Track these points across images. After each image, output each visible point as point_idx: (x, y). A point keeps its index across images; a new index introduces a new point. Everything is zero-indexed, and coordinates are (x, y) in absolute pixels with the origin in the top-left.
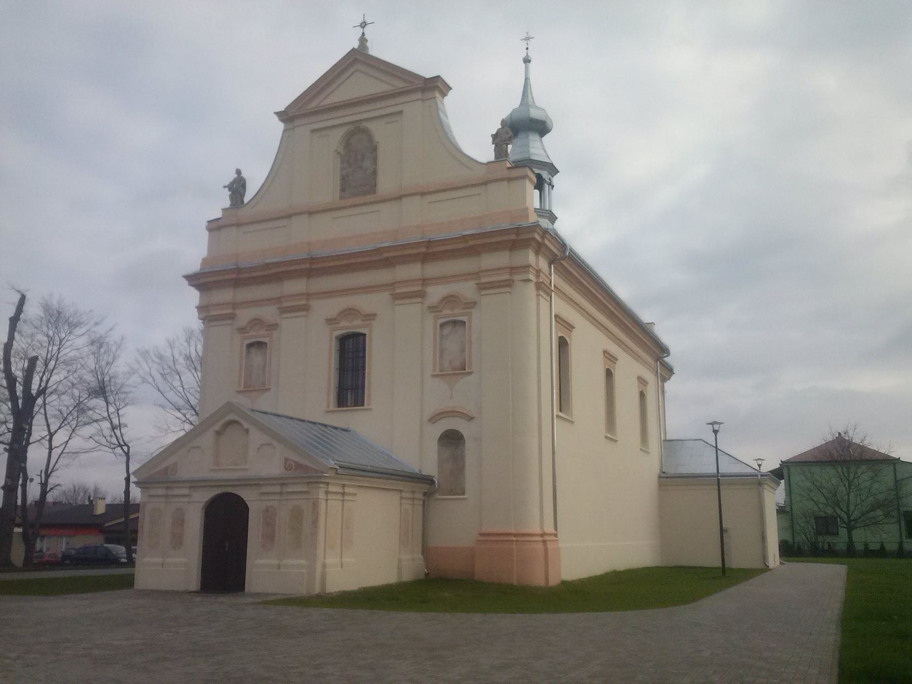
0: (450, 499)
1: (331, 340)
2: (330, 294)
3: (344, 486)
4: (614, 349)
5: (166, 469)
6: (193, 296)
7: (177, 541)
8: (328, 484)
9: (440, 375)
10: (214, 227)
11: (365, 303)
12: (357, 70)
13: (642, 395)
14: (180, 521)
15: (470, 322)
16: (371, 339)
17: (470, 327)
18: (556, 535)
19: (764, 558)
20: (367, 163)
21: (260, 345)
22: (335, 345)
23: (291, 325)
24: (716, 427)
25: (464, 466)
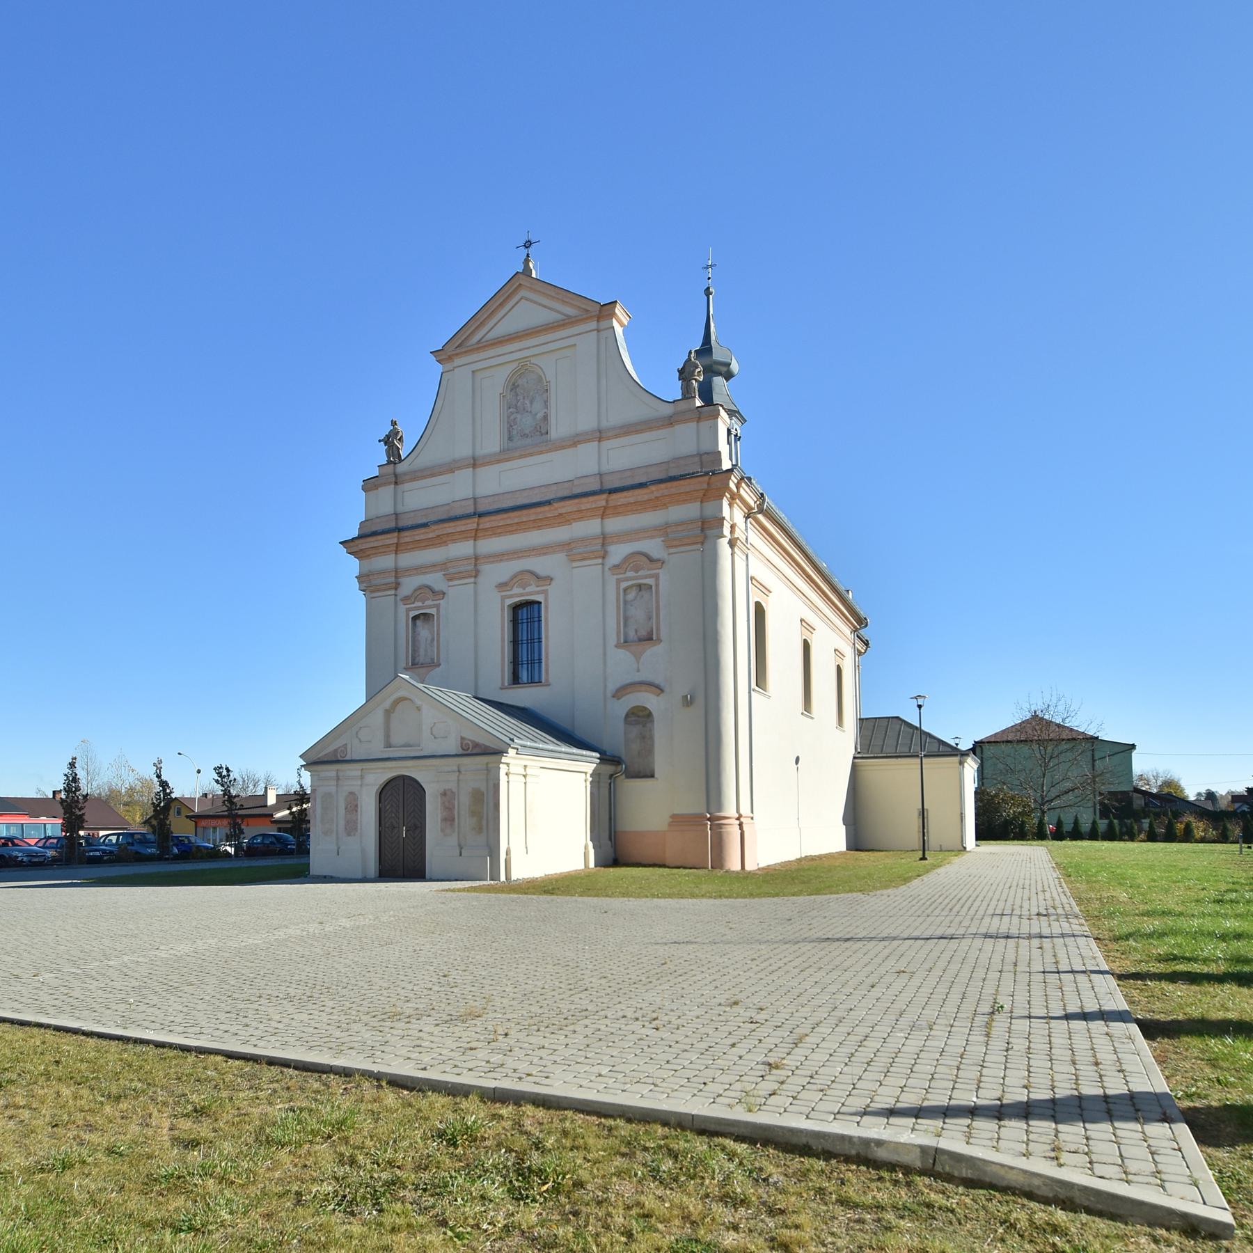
0: (508, 853)
1: (503, 609)
2: (499, 557)
4: (812, 618)
5: (336, 751)
6: (353, 565)
7: (352, 827)
9: (625, 643)
10: (370, 485)
11: (540, 565)
14: (353, 806)
15: (657, 585)
16: (546, 607)
19: (962, 840)
20: (537, 406)
21: (426, 617)
23: (459, 593)
24: (920, 702)
25: (652, 746)
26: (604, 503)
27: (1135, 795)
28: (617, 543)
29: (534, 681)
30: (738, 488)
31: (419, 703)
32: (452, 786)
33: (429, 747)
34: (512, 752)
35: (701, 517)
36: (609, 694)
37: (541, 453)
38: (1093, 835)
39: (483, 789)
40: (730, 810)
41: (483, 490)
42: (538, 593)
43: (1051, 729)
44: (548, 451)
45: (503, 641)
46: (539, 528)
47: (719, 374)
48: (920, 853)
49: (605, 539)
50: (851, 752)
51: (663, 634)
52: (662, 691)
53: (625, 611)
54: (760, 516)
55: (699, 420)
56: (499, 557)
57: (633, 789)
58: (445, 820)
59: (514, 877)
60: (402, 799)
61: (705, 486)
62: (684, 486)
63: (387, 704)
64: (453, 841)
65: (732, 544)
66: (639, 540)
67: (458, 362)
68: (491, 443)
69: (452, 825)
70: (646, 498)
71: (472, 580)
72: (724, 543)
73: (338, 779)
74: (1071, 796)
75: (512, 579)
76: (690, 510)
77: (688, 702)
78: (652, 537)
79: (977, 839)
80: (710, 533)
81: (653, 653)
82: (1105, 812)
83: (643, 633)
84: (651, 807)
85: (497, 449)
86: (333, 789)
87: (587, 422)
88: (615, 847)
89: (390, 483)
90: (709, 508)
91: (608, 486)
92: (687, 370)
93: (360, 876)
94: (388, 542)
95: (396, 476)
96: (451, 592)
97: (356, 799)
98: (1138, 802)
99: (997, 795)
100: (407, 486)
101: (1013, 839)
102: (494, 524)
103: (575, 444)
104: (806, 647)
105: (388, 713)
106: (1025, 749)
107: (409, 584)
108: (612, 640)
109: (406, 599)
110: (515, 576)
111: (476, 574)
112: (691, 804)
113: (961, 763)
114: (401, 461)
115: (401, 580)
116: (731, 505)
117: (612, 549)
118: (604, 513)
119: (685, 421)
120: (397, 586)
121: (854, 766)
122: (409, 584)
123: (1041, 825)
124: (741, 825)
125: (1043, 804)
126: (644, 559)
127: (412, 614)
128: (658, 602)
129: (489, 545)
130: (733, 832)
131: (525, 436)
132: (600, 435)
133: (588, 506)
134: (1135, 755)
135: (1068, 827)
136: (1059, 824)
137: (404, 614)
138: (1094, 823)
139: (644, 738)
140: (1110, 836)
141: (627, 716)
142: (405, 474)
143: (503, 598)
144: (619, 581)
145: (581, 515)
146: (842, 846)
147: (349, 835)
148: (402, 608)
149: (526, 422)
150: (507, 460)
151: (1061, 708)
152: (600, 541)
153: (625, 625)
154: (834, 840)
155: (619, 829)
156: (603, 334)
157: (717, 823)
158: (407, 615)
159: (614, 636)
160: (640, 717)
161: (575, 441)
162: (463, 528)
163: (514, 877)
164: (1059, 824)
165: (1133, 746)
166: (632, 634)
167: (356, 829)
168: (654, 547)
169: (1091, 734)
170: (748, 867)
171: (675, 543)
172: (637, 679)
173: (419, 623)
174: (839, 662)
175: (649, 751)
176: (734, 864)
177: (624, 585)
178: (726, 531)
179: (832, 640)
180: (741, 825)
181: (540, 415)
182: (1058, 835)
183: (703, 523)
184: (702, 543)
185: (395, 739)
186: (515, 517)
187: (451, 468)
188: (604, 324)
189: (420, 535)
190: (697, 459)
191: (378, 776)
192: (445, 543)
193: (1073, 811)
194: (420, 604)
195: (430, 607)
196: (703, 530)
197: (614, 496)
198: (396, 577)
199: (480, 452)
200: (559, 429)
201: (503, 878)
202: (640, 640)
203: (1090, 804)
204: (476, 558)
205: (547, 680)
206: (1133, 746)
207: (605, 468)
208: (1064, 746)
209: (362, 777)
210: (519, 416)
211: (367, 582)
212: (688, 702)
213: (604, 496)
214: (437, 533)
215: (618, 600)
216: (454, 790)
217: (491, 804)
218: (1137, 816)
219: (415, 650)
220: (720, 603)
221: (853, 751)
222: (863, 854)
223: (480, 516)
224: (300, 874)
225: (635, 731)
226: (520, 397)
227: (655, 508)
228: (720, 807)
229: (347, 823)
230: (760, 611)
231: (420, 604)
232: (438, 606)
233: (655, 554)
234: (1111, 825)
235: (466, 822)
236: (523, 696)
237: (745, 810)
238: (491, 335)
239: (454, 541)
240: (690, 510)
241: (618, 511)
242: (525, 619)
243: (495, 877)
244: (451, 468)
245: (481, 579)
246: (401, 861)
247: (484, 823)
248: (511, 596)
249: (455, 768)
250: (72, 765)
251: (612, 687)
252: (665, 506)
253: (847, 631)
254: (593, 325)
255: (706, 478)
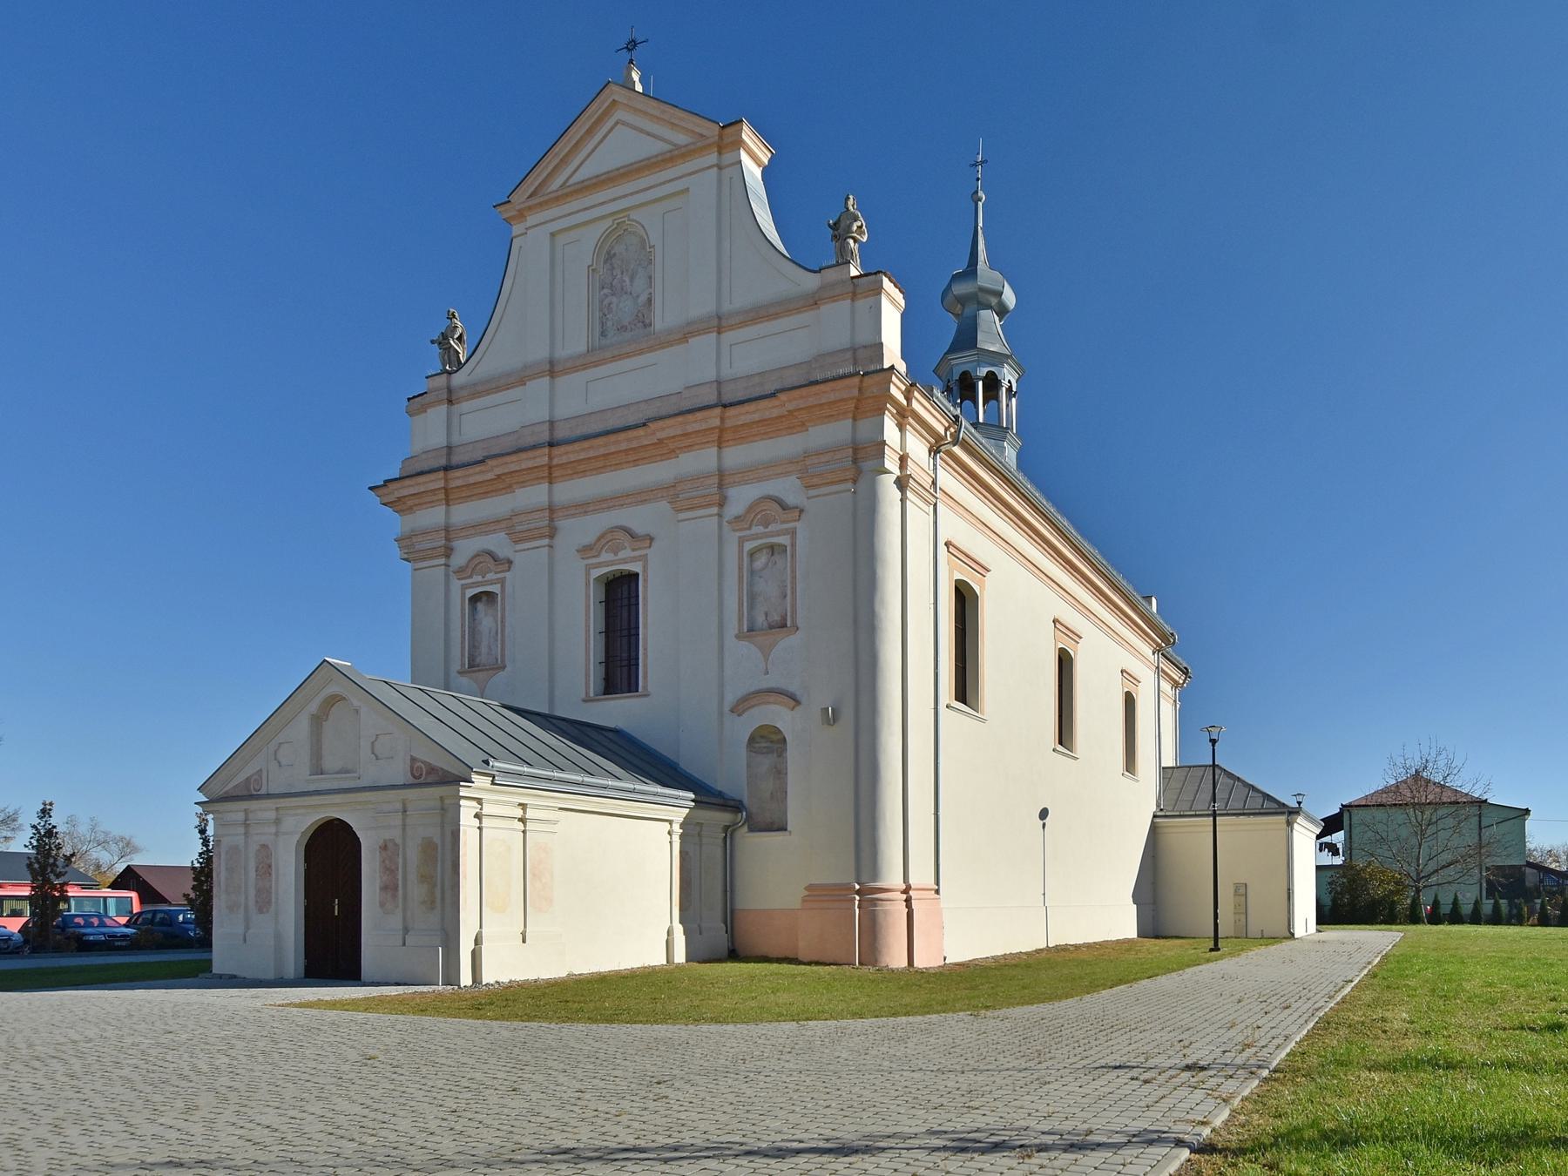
0: (478, 940)
1: (587, 585)
2: (583, 508)
3: (523, 806)
7: (265, 901)
8: (479, 801)
9: (750, 631)
11: (637, 518)
12: (617, 123)
13: (1130, 701)
14: (266, 869)
15: (793, 545)
16: (645, 581)
17: (793, 556)
18: (937, 892)
21: (490, 596)
22: (596, 595)
23: (529, 559)
26: (717, 422)
27: (1528, 870)
28: (739, 483)
29: (631, 686)
30: (908, 399)
31: (356, 703)
32: (395, 834)
33: (371, 773)
34: (480, 781)
35: (854, 441)
36: (727, 709)
37: (641, 352)
38: (1476, 918)
39: (437, 840)
40: (892, 877)
41: (562, 411)
42: (634, 559)
43: (1431, 787)
44: (651, 349)
45: (587, 631)
46: (636, 463)
47: (989, 307)
48: (1211, 945)
49: (723, 478)
50: (1153, 808)
51: (799, 622)
52: (798, 702)
53: (751, 585)
54: (957, 450)
55: (854, 296)
56: (583, 508)
57: (753, 844)
58: (384, 888)
59: (488, 977)
60: (332, 856)
61: (855, 392)
62: (828, 393)
63: (313, 707)
64: (396, 921)
65: (902, 484)
66: (768, 478)
67: (532, 219)
68: (576, 342)
69: (395, 896)
70: (775, 413)
71: (546, 541)
72: (887, 484)
73: (246, 825)
74: (1451, 870)
75: (599, 539)
76: (838, 432)
77: (831, 718)
78: (787, 474)
79: (1319, 922)
80: (867, 465)
81: (787, 644)
82: (1492, 890)
83: (776, 618)
84: (778, 875)
85: (583, 348)
86: (240, 840)
87: (701, 305)
88: (723, 928)
89: (439, 402)
90: (865, 426)
91: (727, 398)
92: (842, 225)
93: (271, 976)
94: (432, 486)
95: (450, 390)
96: (518, 559)
97: (269, 856)
98: (1531, 877)
99: (1363, 870)
100: (465, 406)
101: (1381, 923)
102: (573, 457)
103: (684, 338)
104: (1065, 663)
105: (318, 721)
106: (1399, 815)
107: (465, 548)
108: (732, 627)
109: (460, 571)
110: (602, 536)
111: (552, 533)
112: (834, 870)
113: (1290, 824)
114: (460, 366)
115: (455, 544)
116: (901, 427)
117: (732, 492)
118: (721, 439)
119: (834, 299)
120: (448, 552)
121: (1154, 829)
122: (465, 548)
123: (1415, 904)
124: (908, 901)
125: (1418, 881)
126: (776, 506)
127: (470, 593)
128: (793, 571)
129: (570, 490)
130: (895, 911)
131: (623, 329)
132: (719, 324)
133: (697, 427)
134: (1530, 824)
135: (1445, 909)
136: (1436, 904)
137: (460, 592)
138: (1477, 903)
139: (779, 772)
140: (1496, 919)
141: (752, 740)
142: (462, 388)
143: (588, 568)
144: (742, 541)
145: (688, 442)
146: (1131, 932)
147: (261, 911)
148: (456, 585)
149: (625, 308)
150: (596, 364)
151: (1441, 763)
152: (715, 480)
153: (751, 607)
154: (1122, 923)
155: (739, 905)
156: (727, 172)
157: (870, 896)
158: (463, 595)
159: (735, 622)
160: (768, 742)
161: (685, 334)
162: (530, 464)
163: (488, 977)
164: (1436, 904)
165: (1527, 811)
166: (760, 620)
167: (269, 902)
168: (788, 488)
169: (1476, 795)
170: (919, 963)
171: (815, 481)
172: (765, 685)
173: (480, 606)
174: (1130, 687)
175: (781, 794)
176: (896, 958)
177: (748, 546)
178: (891, 463)
179: (1116, 657)
180: (908, 901)
181: (643, 298)
182: (1435, 919)
183: (855, 450)
184: (855, 482)
185: (329, 763)
186: (600, 447)
187: (520, 378)
188: (728, 158)
189: (476, 475)
190: (849, 355)
191: (302, 820)
192: (509, 488)
193: (1453, 887)
194: (479, 578)
195: (492, 583)
196: (855, 461)
197: (731, 412)
198: (448, 539)
199: (561, 353)
200: (665, 318)
201: (466, 979)
202: (771, 627)
203: (1476, 878)
204: (551, 509)
205: (645, 687)
206: (1527, 811)
207: (727, 372)
208: (1442, 812)
209: (277, 822)
210: (614, 300)
211: (412, 548)
212: (831, 718)
213: (718, 411)
214: (498, 471)
215: (740, 568)
216: (399, 841)
217: (448, 864)
218: (1529, 895)
219: (474, 647)
220: (879, 571)
221: (1154, 808)
222: (1162, 942)
223: (553, 449)
224: (199, 973)
225: (765, 762)
226: (617, 272)
227: (791, 430)
228: (875, 873)
229: (259, 891)
230: (965, 600)
231: (479, 578)
232: (502, 582)
233: (791, 500)
234: (1496, 907)
235: (417, 891)
236: (615, 712)
237: (921, 875)
238: (578, 177)
239: (522, 484)
240: (838, 432)
241: (743, 434)
242: (620, 595)
243: (452, 977)
244: (520, 378)
245: (558, 540)
246: (331, 953)
247: (438, 895)
248: (599, 565)
249: (399, 806)
250: (45, 812)
251: (730, 699)
252: (803, 426)
253: (1147, 650)
254: (712, 158)
255: (856, 380)
